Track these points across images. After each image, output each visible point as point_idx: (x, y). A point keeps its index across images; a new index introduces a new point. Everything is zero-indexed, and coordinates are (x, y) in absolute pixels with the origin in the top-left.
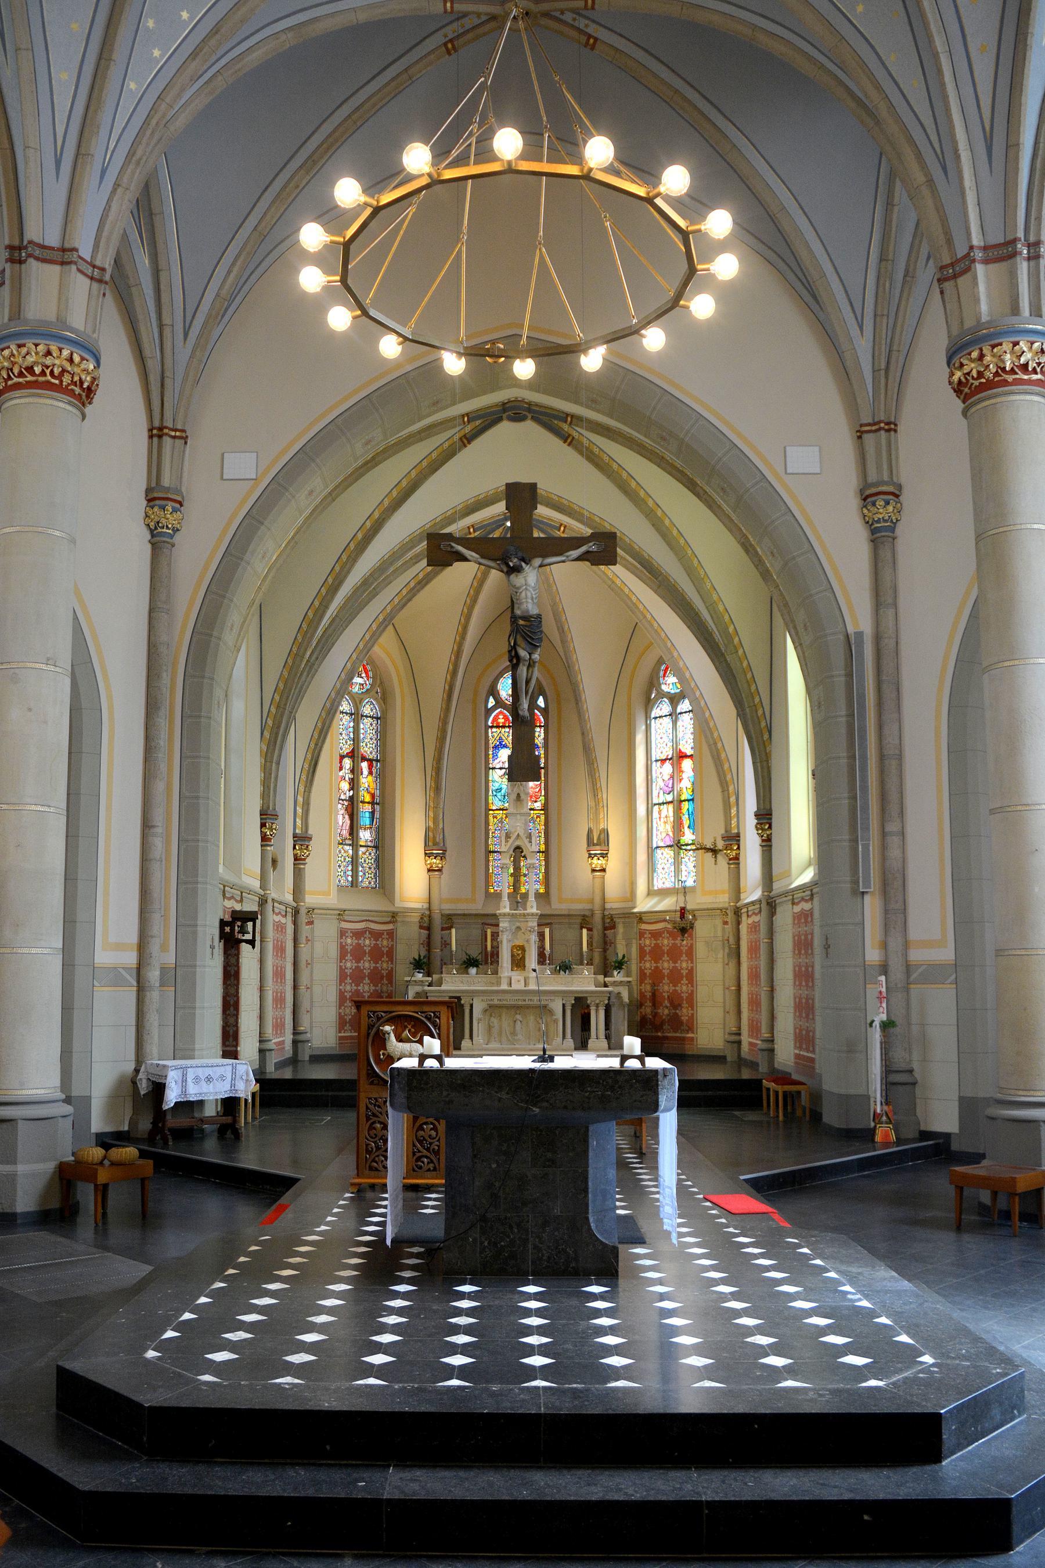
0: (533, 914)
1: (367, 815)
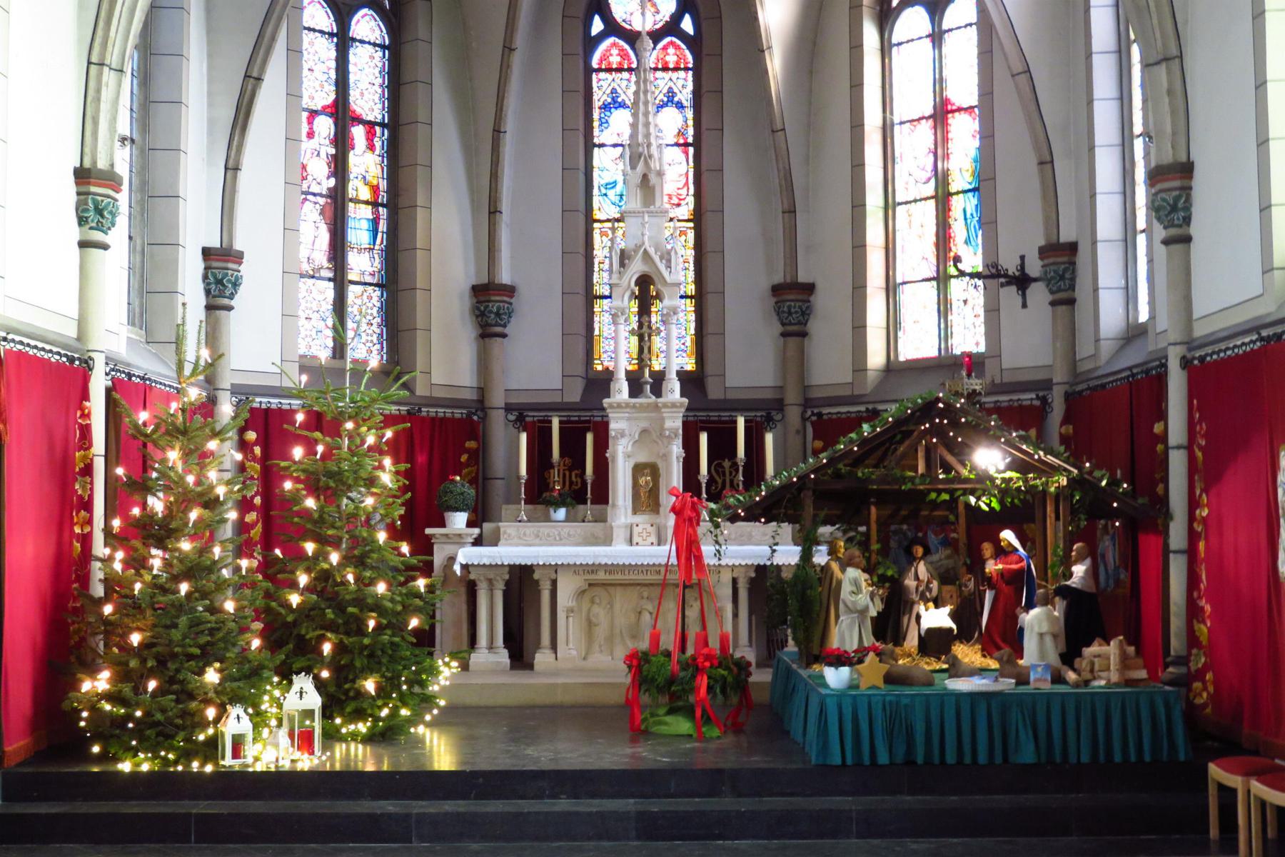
0: (674, 405)
1: (365, 225)
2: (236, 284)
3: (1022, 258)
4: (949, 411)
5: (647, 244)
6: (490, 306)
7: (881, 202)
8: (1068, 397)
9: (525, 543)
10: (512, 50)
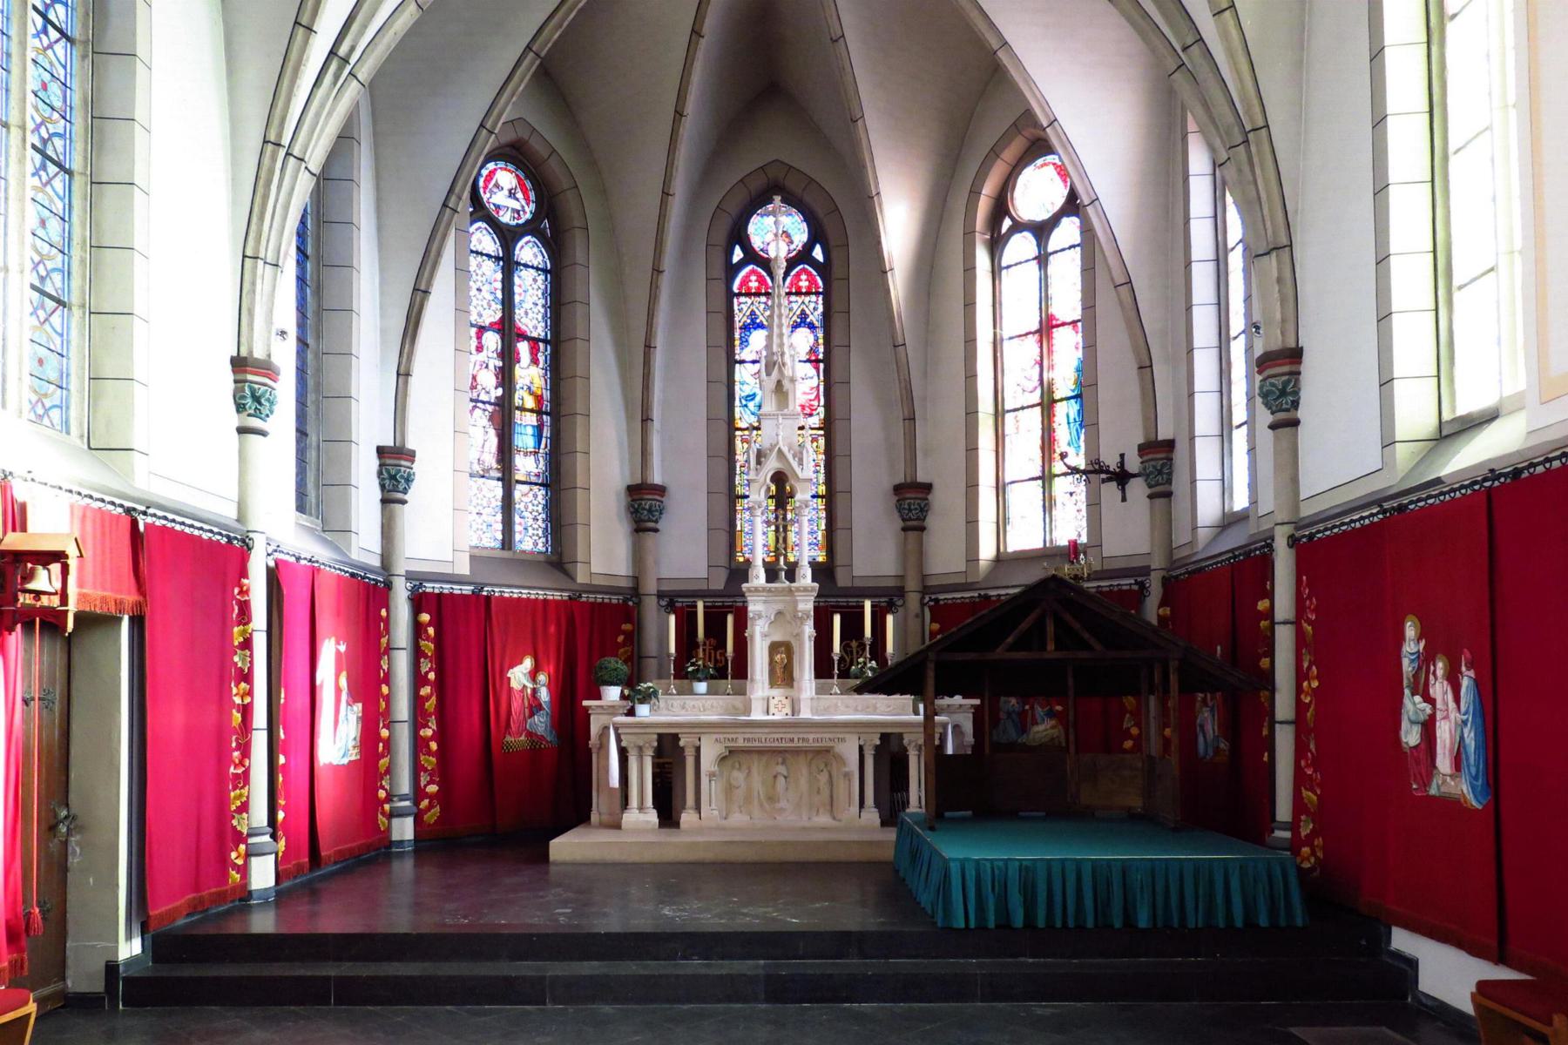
0: (805, 589)
1: (530, 431)
2: (409, 480)
3: (1122, 456)
5: (781, 444)
6: (644, 505)
7: (991, 410)
8: (1166, 582)
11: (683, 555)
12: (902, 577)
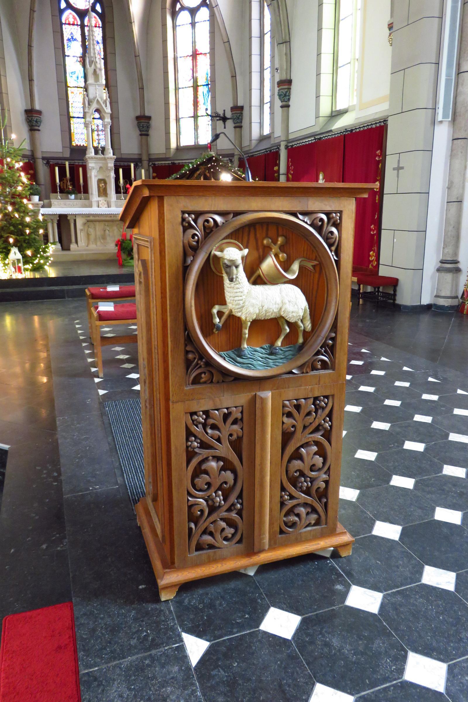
0: (111, 158)
3: (224, 111)
4: (217, 160)
5: (98, 98)
7: (174, 88)
9: (61, 206)
10: (34, 11)
11: (50, 143)
12: (140, 154)
